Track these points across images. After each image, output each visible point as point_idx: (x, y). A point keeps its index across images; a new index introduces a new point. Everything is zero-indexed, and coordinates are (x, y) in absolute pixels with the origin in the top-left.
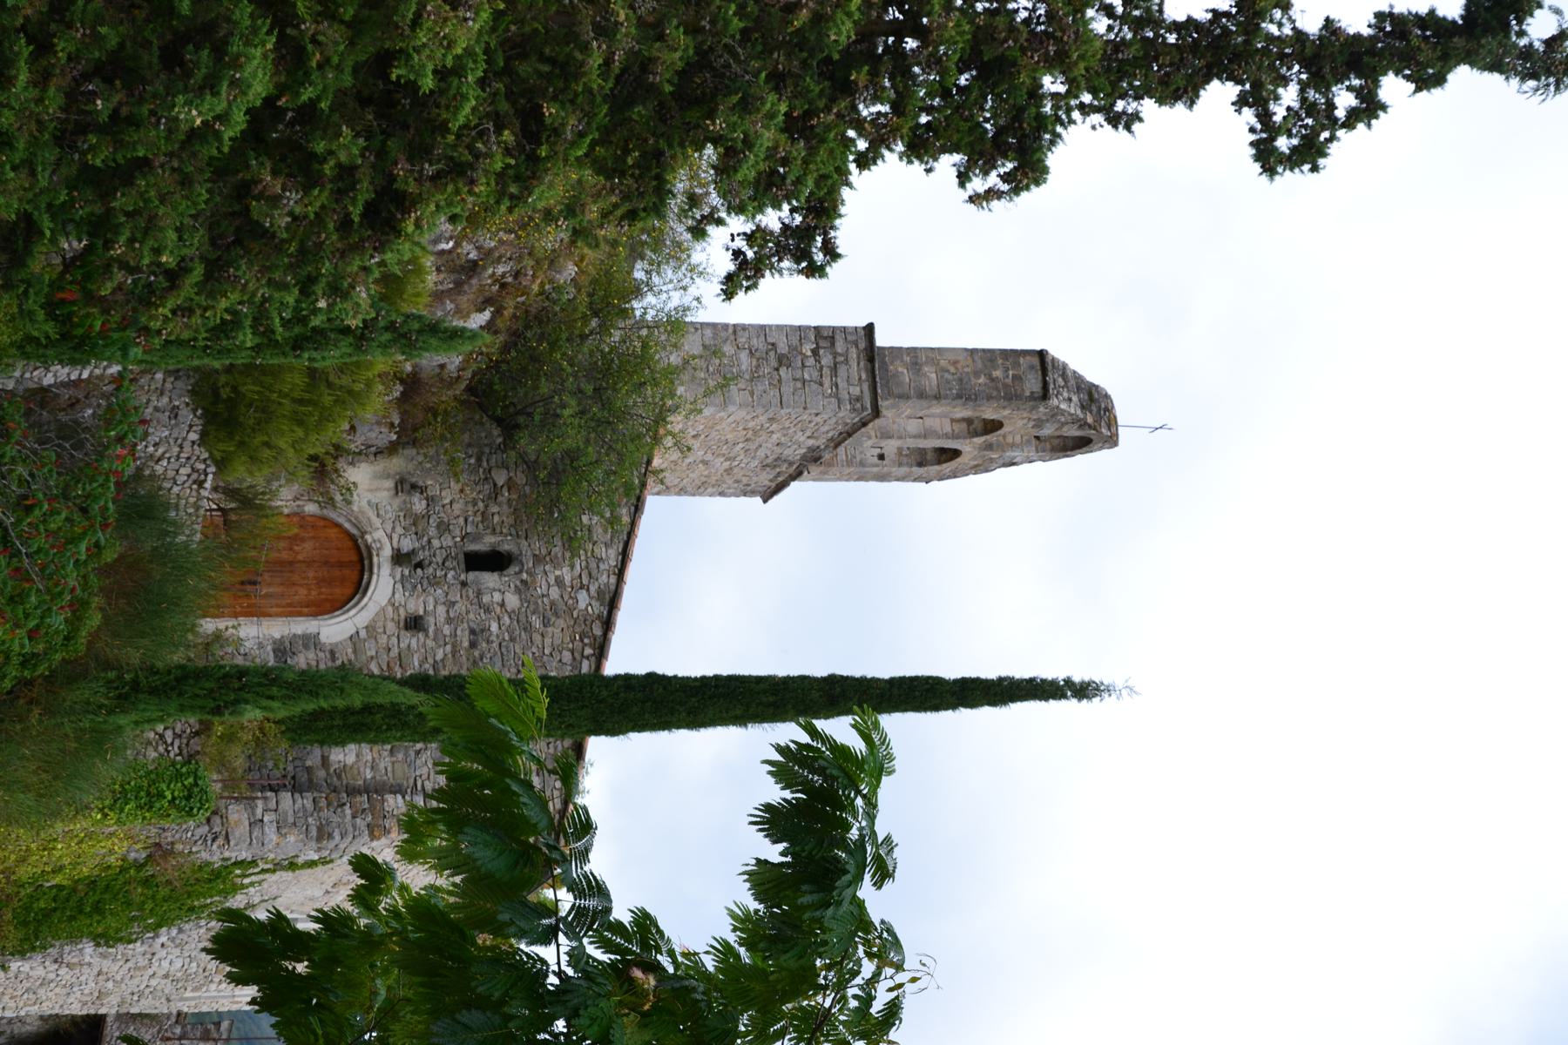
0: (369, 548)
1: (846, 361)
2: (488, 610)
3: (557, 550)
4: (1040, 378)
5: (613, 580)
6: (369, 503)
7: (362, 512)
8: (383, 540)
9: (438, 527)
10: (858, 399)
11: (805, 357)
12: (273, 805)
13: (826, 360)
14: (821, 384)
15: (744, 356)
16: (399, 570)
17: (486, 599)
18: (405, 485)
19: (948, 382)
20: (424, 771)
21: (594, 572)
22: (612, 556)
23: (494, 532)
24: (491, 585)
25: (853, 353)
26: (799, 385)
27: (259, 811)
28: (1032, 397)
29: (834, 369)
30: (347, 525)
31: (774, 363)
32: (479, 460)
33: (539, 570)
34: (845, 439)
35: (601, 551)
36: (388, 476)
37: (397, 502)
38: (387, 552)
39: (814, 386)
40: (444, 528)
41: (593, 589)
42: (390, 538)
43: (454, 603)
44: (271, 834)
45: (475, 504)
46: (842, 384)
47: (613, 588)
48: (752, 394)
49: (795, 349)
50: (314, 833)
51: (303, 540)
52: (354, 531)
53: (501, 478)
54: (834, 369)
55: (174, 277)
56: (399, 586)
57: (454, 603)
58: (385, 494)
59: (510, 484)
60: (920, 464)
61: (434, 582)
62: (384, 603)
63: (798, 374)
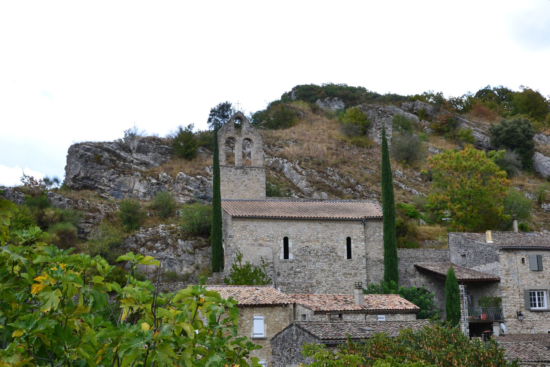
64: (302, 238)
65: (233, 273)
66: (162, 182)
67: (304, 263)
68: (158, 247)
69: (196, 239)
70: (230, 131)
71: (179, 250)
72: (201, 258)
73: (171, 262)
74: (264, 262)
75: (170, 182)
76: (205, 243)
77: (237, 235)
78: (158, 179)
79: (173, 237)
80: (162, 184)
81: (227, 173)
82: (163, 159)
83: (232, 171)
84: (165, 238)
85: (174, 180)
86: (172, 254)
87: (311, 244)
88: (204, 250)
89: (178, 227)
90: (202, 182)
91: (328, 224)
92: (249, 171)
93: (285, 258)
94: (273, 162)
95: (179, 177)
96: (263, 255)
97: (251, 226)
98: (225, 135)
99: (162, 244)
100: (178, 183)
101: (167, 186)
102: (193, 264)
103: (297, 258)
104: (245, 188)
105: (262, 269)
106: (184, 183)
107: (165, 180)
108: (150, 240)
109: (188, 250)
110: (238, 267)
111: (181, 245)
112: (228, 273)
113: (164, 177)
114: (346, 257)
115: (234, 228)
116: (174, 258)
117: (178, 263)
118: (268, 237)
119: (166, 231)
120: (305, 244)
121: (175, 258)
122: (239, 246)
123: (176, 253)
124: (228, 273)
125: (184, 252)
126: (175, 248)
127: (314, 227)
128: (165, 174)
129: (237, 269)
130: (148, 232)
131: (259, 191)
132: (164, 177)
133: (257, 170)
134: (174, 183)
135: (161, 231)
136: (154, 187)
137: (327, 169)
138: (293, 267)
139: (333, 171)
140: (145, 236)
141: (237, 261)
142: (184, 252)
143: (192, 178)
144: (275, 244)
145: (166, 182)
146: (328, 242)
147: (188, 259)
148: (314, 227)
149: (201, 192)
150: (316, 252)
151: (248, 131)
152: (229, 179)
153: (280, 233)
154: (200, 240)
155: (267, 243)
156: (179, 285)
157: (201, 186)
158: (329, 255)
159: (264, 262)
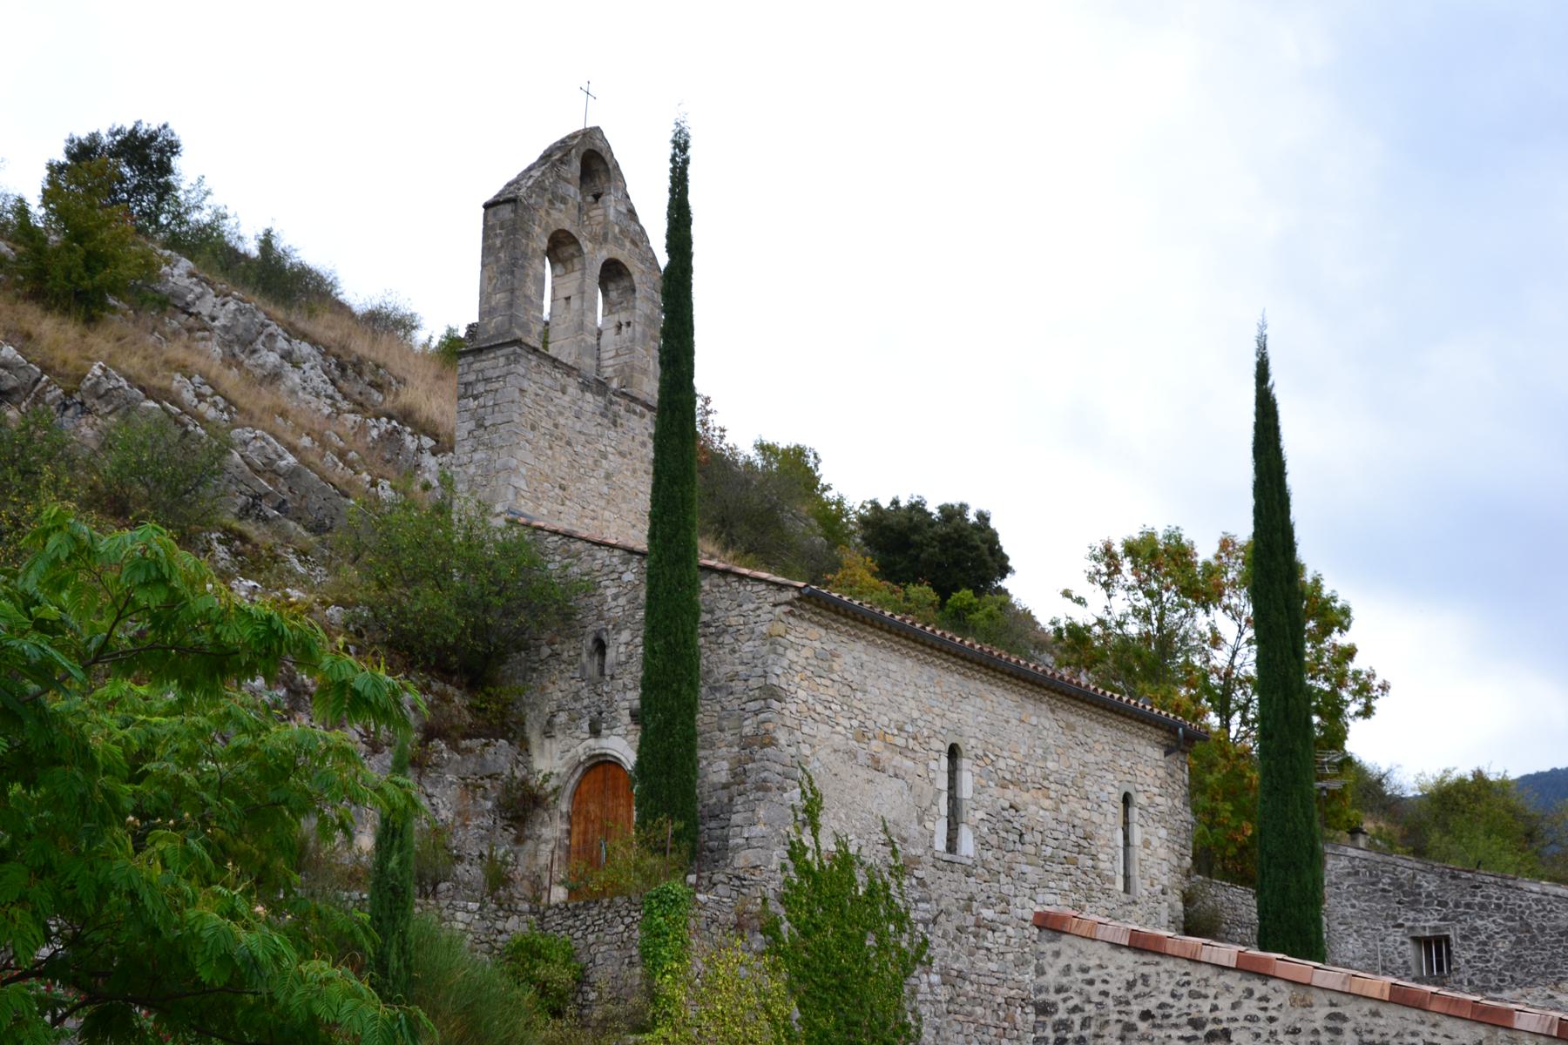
0: (591, 757)
1: (482, 371)
2: (630, 656)
3: (594, 601)
4: (502, 206)
5: (617, 552)
6: (561, 759)
7: (567, 763)
8: (584, 746)
9: (576, 701)
10: (508, 358)
11: (479, 406)
12: (738, 829)
13: (480, 388)
14: (497, 390)
15: (477, 456)
16: (604, 732)
17: (623, 658)
18: (548, 733)
19: (502, 284)
20: (736, 702)
21: (611, 568)
22: (602, 554)
23: (579, 655)
24: (614, 654)
25: (477, 366)
26: (497, 409)
27: (741, 841)
28: (514, 211)
29: (487, 380)
30: (577, 776)
31: (482, 431)
32: (534, 670)
33: (606, 615)
34: (562, 363)
35: (597, 564)
36: (542, 744)
37: (560, 736)
38: (591, 742)
39: (498, 395)
40: (577, 697)
41: (622, 568)
42: (584, 740)
43: (624, 685)
44: (759, 829)
45: (561, 672)
46: (497, 373)
47: (622, 552)
48: (502, 447)
49: (473, 415)
50: (760, 794)
51: (588, 812)
52: (580, 770)
53: (546, 651)
54: (487, 380)
55: (1268, 867)
56: (614, 731)
57: (624, 685)
58: (554, 746)
59: (551, 643)
60: (634, 290)
61: (610, 703)
62: (625, 742)
63: (489, 410)
64: (1001, 764)
70: (564, 200)
72: (453, 793)
74: (894, 853)
75: (39, 398)
76: (468, 718)
81: (552, 394)
83: (570, 390)
85: (68, 394)
87: (1026, 797)
88: (470, 750)
91: (1072, 719)
92: (622, 412)
94: (380, 436)
97: (848, 659)
98: (548, 213)
100: (85, 410)
104: (605, 489)
105: (893, 884)
110: (809, 856)
112: (772, 885)
115: (791, 654)
120: (1011, 794)
122: (806, 750)
124: (772, 885)
127: (1034, 720)
129: (805, 871)
134: (66, 407)
138: (971, 899)
143: (151, 404)
144: (921, 770)
148: (1034, 720)
150: (1038, 837)
151: (621, 231)
152: (556, 426)
154: (443, 697)
158: (1074, 862)
159: (894, 853)
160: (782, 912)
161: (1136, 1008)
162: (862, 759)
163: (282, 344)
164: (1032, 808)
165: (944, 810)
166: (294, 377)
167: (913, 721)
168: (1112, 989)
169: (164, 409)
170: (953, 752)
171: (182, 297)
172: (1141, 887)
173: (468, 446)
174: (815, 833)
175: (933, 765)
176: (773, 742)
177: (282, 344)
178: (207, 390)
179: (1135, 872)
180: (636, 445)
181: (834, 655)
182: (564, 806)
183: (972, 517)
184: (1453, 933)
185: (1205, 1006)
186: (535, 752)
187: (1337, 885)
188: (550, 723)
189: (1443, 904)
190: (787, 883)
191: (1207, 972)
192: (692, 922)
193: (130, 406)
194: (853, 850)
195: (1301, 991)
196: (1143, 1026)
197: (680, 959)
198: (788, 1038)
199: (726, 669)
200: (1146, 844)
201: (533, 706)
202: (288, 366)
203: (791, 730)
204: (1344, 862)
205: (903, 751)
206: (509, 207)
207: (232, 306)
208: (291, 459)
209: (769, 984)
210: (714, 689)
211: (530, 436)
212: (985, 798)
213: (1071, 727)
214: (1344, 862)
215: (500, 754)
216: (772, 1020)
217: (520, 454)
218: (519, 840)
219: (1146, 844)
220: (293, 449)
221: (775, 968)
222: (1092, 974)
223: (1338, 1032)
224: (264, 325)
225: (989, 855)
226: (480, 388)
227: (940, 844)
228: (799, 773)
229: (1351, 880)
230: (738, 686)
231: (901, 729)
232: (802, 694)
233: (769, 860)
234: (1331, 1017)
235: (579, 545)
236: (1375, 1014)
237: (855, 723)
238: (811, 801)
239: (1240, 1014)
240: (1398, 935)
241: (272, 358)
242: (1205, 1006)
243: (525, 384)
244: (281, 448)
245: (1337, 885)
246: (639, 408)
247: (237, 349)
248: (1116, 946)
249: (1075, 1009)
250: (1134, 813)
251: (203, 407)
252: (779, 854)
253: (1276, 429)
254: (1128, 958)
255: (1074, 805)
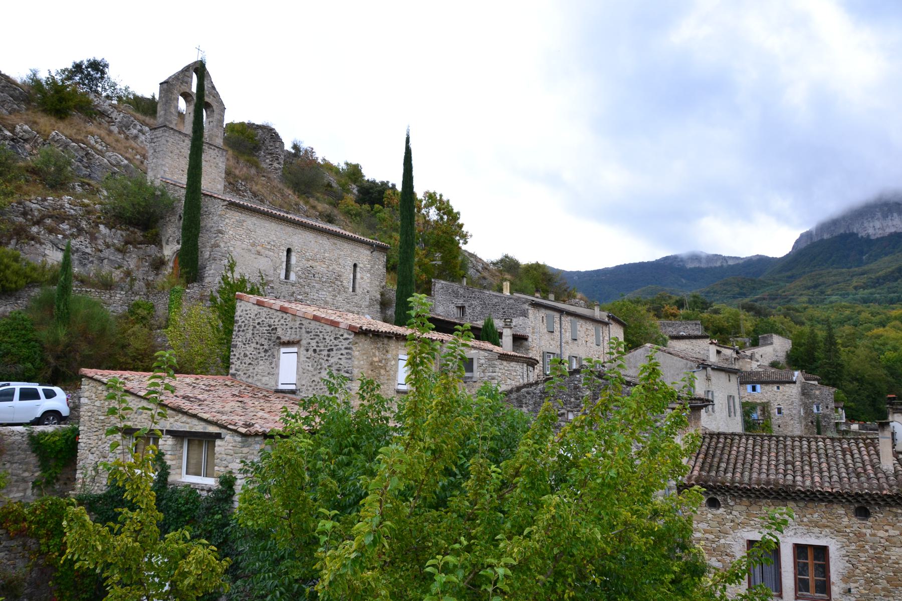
13: (155, 140)
18: (167, 244)
29: (157, 138)
40: (174, 233)
44: (212, 271)
53: (168, 219)
54: (157, 138)
64: (308, 254)
65: (222, 288)
66: (20, 138)
67: (307, 289)
68: (64, 230)
69: (128, 230)
71: (100, 242)
72: (135, 260)
73: (85, 259)
74: (262, 279)
75: (36, 141)
76: (142, 238)
77: (231, 232)
78: (13, 130)
79: (89, 219)
80: (19, 142)
82: (15, 106)
83: (186, 141)
84: (77, 219)
85: (45, 140)
86: (88, 245)
87: (316, 264)
88: (141, 248)
89: (97, 206)
90: (87, 154)
91: (336, 242)
93: (286, 279)
95: (54, 137)
96: (262, 268)
99: (72, 227)
101: (27, 146)
102: (120, 267)
103: (300, 280)
106: (60, 148)
107: (27, 136)
108: (51, 217)
109: (114, 245)
110: (229, 279)
111: (104, 236)
113: (24, 131)
114: (351, 290)
115: (227, 221)
116: (90, 252)
117: (96, 262)
118: (269, 243)
119: (77, 208)
120: (310, 263)
121: (93, 254)
122: (231, 249)
123: (94, 246)
125: (108, 246)
126: (93, 238)
127: (321, 242)
128: (26, 127)
129: (228, 284)
130: (46, 203)
131: (216, 180)
132: (24, 131)
133: (216, 151)
134: (44, 145)
135: (67, 205)
136: (7, 142)
137: (237, 181)
138: (294, 293)
139: (245, 186)
140: (39, 207)
141: (229, 270)
142: (108, 246)
143: (74, 144)
144: (276, 255)
145: (26, 141)
146: (334, 266)
147: (113, 258)
148: (321, 242)
149: (84, 169)
150: (321, 276)
153: (283, 242)
155: (267, 252)
156: (118, 295)
157: (85, 160)
158: (334, 283)
159: (262, 279)
160: (218, 296)
161: (257, 322)
162: (253, 252)
163: (138, 127)
164: (319, 267)
165: (284, 266)
166: (142, 138)
167: (274, 241)
168: (252, 317)
169: (80, 146)
170: (289, 251)
171: (107, 112)
172: (358, 290)
173: (152, 157)
174: (232, 273)
175: (281, 254)
176: (218, 246)
177: (138, 127)
178: (99, 140)
179: (357, 286)
180: (212, 158)
181: (244, 221)
182: (171, 265)
183: (390, 185)
184: (466, 305)
185: (272, 321)
186: (164, 249)
187: (438, 291)
188: (168, 240)
189: (464, 297)
190: (221, 287)
191: (273, 311)
192: (183, 298)
193: (66, 146)
194: (246, 278)
195: (294, 317)
196: (258, 327)
197: (178, 308)
198: (217, 331)
199: (210, 225)
200: (362, 278)
201: (164, 235)
202: (140, 134)
203: (226, 243)
204: (440, 285)
205: (269, 250)
206: (166, 84)
207: (122, 115)
208: (126, 162)
209: (211, 316)
210: (207, 231)
211: (170, 155)
212: (301, 264)
213: (335, 244)
214: (440, 285)
215: (152, 249)
216: (212, 326)
217: (166, 160)
218: (157, 274)
219: (362, 278)
220: (126, 158)
221: (214, 311)
222: (248, 312)
223: (301, 328)
224: (133, 121)
225: (300, 280)
226: (155, 140)
227: (283, 277)
228: (228, 255)
229: (442, 290)
230: (212, 230)
231: (269, 243)
232: (231, 232)
233: (214, 280)
234: (301, 324)
235: (177, 188)
236: (310, 323)
237: (251, 241)
238: (231, 264)
239: (280, 323)
240: (453, 306)
241: (135, 132)
242: (272, 321)
243: (168, 139)
244: (122, 158)
245: (438, 291)
246: (213, 147)
247: (124, 129)
248: (254, 304)
249: (243, 322)
250: (358, 269)
251: (97, 145)
252: (218, 279)
253: (411, 158)
254: (256, 307)
255: (334, 266)
